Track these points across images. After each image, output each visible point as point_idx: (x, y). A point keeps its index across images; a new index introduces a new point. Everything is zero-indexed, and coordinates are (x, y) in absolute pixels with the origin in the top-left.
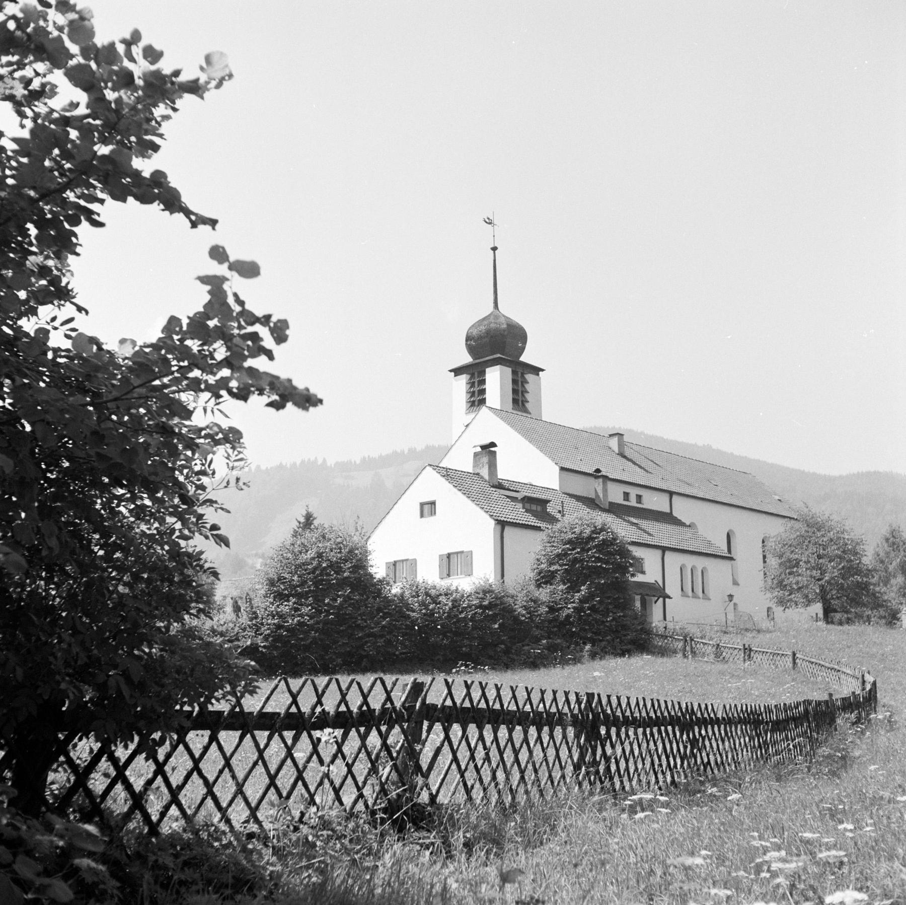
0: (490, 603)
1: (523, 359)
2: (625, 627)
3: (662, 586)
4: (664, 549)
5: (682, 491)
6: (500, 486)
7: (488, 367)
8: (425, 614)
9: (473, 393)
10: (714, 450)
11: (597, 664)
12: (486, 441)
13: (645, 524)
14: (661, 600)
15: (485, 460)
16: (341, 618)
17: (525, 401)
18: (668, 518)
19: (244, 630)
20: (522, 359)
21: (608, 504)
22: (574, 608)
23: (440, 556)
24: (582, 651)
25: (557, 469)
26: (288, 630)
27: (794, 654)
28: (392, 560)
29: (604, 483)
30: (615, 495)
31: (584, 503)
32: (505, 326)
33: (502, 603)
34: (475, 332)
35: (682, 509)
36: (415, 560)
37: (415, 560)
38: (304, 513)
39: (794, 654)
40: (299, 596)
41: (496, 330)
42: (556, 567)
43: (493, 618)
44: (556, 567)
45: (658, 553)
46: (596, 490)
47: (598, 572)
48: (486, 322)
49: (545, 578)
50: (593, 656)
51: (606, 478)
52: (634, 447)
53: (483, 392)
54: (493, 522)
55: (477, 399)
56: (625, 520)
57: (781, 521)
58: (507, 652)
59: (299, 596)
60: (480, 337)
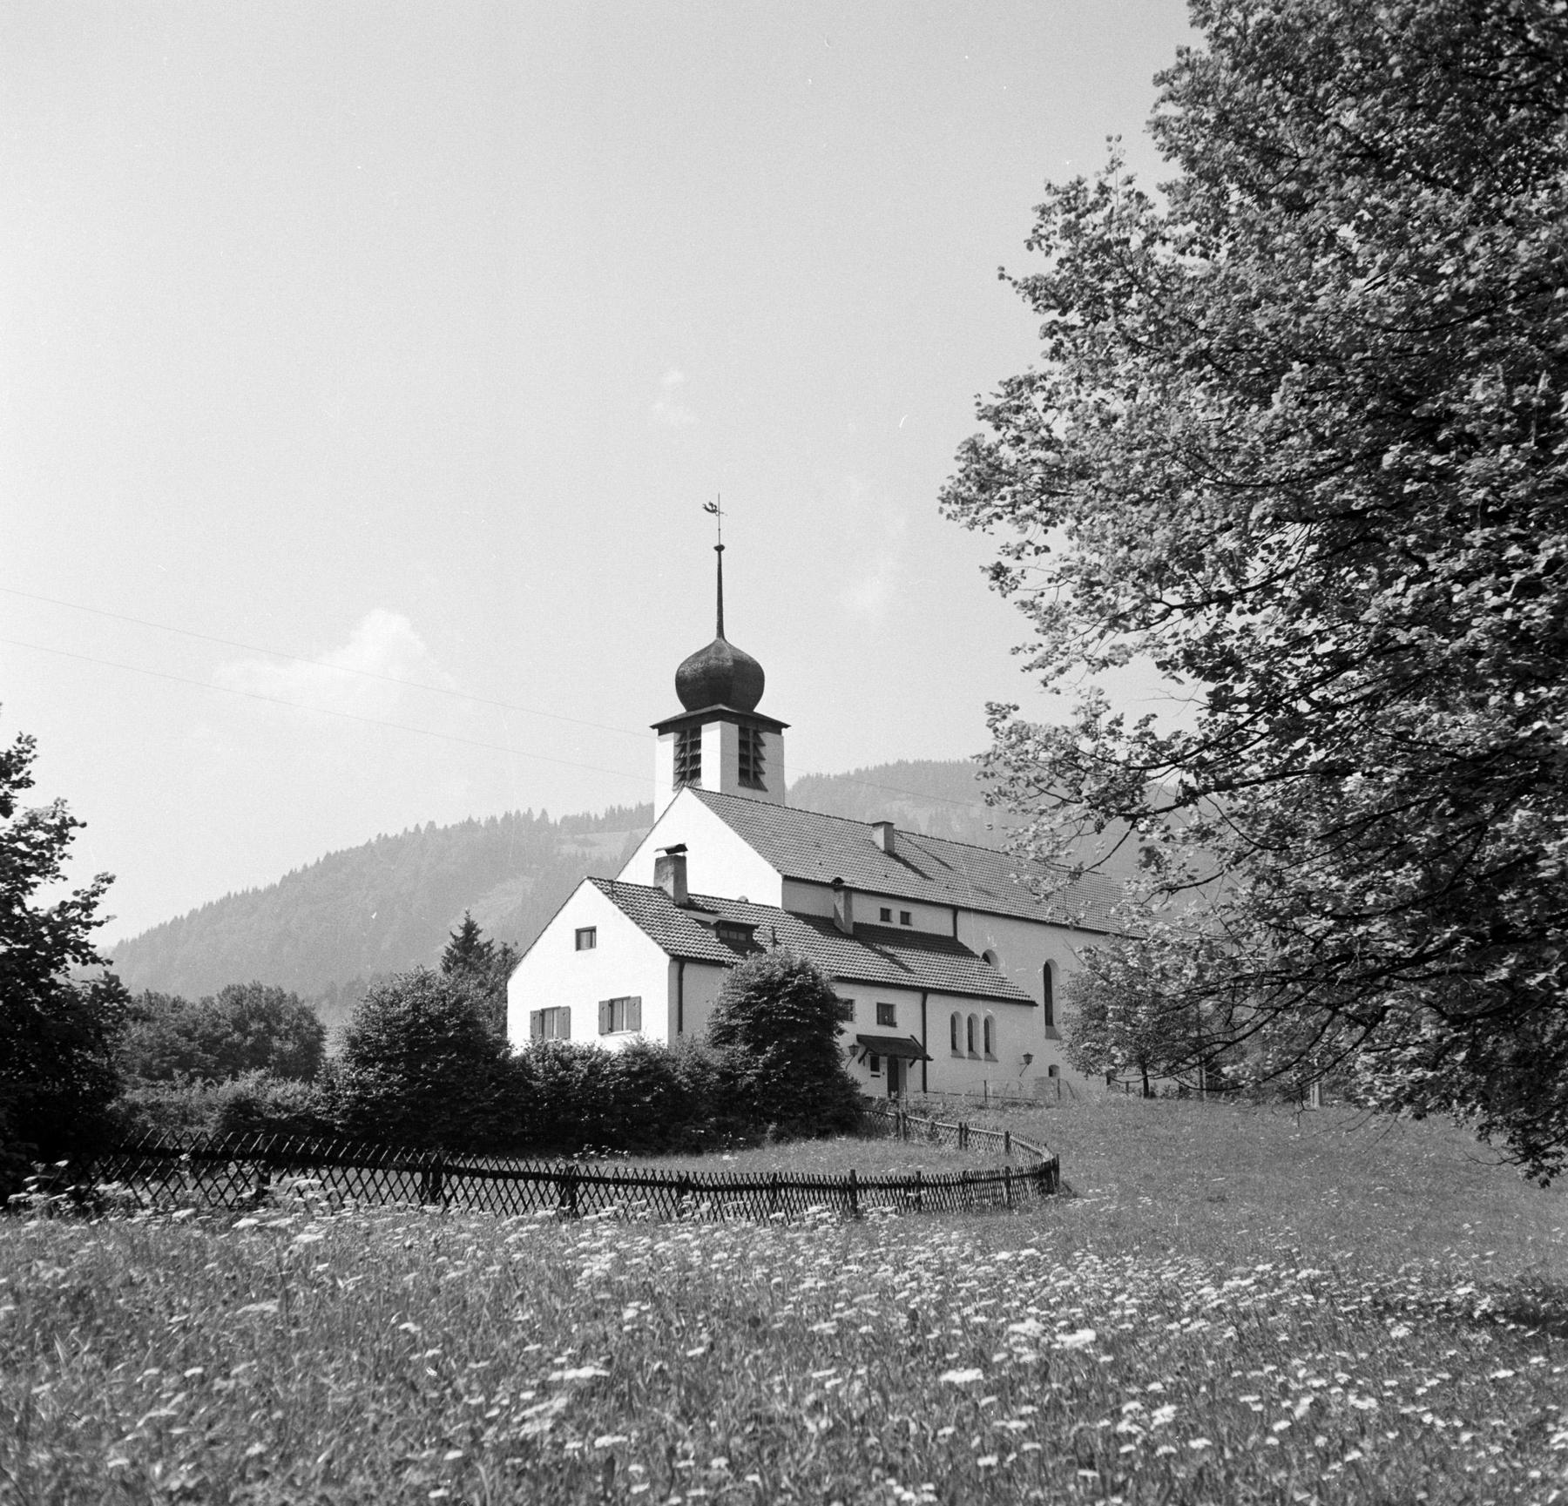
1: (759, 709)
4: (925, 992)
5: (973, 904)
8: (552, 1084)
9: (684, 759)
12: (673, 843)
13: (904, 955)
14: (919, 1063)
15: (670, 869)
17: (758, 773)
18: (949, 946)
19: (317, 1104)
20: (759, 709)
24: (764, 1132)
25: (779, 878)
26: (372, 1103)
27: (1007, 1135)
28: (539, 1008)
29: (848, 899)
30: (866, 912)
32: (730, 663)
33: (657, 1069)
34: (688, 671)
35: (973, 933)
36: (568, 1008)
37: (568, 1008)
38: (463, 923)
39: (1007, 1135)
40: (388, 1060)
41: (718, 668)
42: (739, 1021)
43: (647, 1088)
44: (739, 1021)
45: (918, 996)
47: (791, 1027)
49: (724, 1036)
50: (779, 1138)
51: (851, 891)
52: (913, 839)
54: (667, 958)
55: (688, 770)
56: (874, 950)
58: (662, 1133)
59: (388, 1060)
60: (695, 680)
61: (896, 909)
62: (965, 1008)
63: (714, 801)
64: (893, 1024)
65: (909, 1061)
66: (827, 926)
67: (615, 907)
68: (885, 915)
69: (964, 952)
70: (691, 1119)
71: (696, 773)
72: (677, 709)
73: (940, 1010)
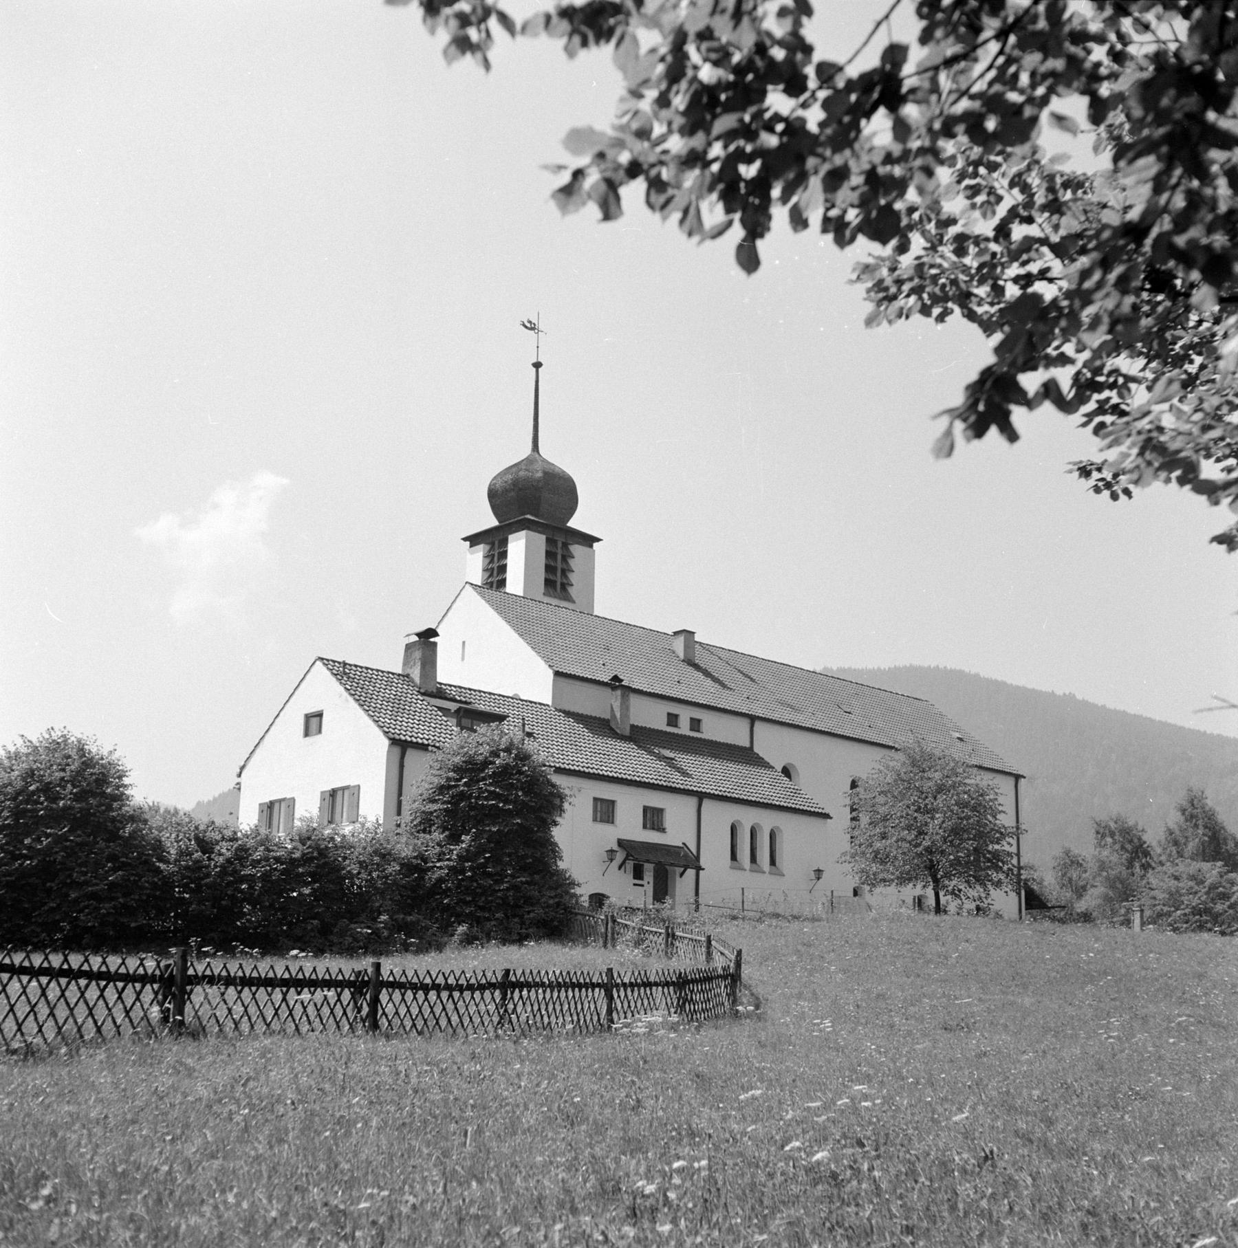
0: (304, 855)
1: (573, 523)
2: (529, 901)
3: (694, 852)
4: (701, 796)
6: (440, 693)
7: (511, 533)
8: (187, 868)
9: (492, 569)
10: (1110, 710)
11: (470, 952)
12: (422, 628)
13: (686, 760)
14: (691, 873)
15: (418, 654)
16: (47, 869)
17: (565, 586)
18: (746, 756)
20: (573, 523)
21: (628, 729)
22: (450, 868)
23: (322, 793)
25: (550, 673)
27: (709, 938)
29: (625, 698)
30: (651, 716)
31: (586, 726)
34: (499, 484)
35: (769, 743)
36: (293, 800)
37: (293, 800)
41: (527, 479)
45: (693, 801)
46: (612, 708)
47: (494, 814)
48: (514, 470)
49: (425, 824)
50: (468, 940)
53: (503, 569)
54: (386, 742)
55: (495, 577)
56: (651, 753)
57: (878, 753)
61: (685, 715)
62: (748, 817)
63: (512, 612)
64: (662, 830)
65: (679, 870)
66: (601, 726)
67: (341, 689)
68: (673, 719)
69: (759, 762)
70: (363, 917)
71: (502, 583)
72: (490, 521)
73: (718, 818)
